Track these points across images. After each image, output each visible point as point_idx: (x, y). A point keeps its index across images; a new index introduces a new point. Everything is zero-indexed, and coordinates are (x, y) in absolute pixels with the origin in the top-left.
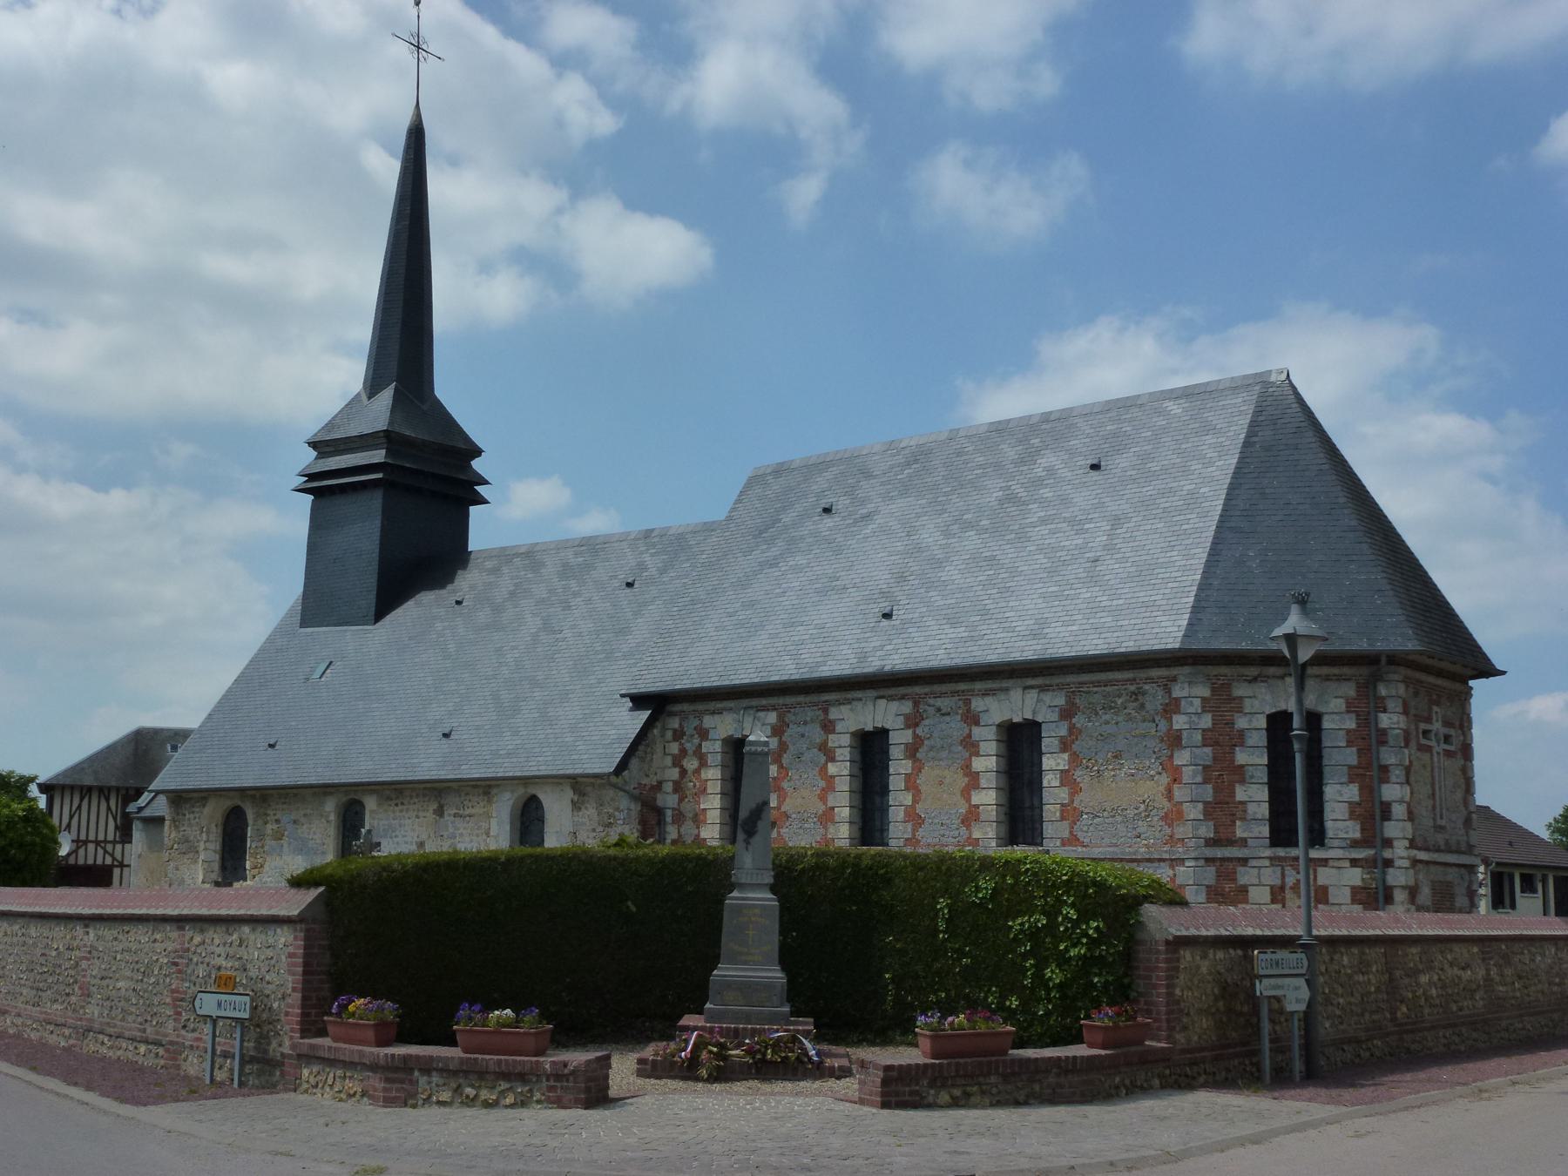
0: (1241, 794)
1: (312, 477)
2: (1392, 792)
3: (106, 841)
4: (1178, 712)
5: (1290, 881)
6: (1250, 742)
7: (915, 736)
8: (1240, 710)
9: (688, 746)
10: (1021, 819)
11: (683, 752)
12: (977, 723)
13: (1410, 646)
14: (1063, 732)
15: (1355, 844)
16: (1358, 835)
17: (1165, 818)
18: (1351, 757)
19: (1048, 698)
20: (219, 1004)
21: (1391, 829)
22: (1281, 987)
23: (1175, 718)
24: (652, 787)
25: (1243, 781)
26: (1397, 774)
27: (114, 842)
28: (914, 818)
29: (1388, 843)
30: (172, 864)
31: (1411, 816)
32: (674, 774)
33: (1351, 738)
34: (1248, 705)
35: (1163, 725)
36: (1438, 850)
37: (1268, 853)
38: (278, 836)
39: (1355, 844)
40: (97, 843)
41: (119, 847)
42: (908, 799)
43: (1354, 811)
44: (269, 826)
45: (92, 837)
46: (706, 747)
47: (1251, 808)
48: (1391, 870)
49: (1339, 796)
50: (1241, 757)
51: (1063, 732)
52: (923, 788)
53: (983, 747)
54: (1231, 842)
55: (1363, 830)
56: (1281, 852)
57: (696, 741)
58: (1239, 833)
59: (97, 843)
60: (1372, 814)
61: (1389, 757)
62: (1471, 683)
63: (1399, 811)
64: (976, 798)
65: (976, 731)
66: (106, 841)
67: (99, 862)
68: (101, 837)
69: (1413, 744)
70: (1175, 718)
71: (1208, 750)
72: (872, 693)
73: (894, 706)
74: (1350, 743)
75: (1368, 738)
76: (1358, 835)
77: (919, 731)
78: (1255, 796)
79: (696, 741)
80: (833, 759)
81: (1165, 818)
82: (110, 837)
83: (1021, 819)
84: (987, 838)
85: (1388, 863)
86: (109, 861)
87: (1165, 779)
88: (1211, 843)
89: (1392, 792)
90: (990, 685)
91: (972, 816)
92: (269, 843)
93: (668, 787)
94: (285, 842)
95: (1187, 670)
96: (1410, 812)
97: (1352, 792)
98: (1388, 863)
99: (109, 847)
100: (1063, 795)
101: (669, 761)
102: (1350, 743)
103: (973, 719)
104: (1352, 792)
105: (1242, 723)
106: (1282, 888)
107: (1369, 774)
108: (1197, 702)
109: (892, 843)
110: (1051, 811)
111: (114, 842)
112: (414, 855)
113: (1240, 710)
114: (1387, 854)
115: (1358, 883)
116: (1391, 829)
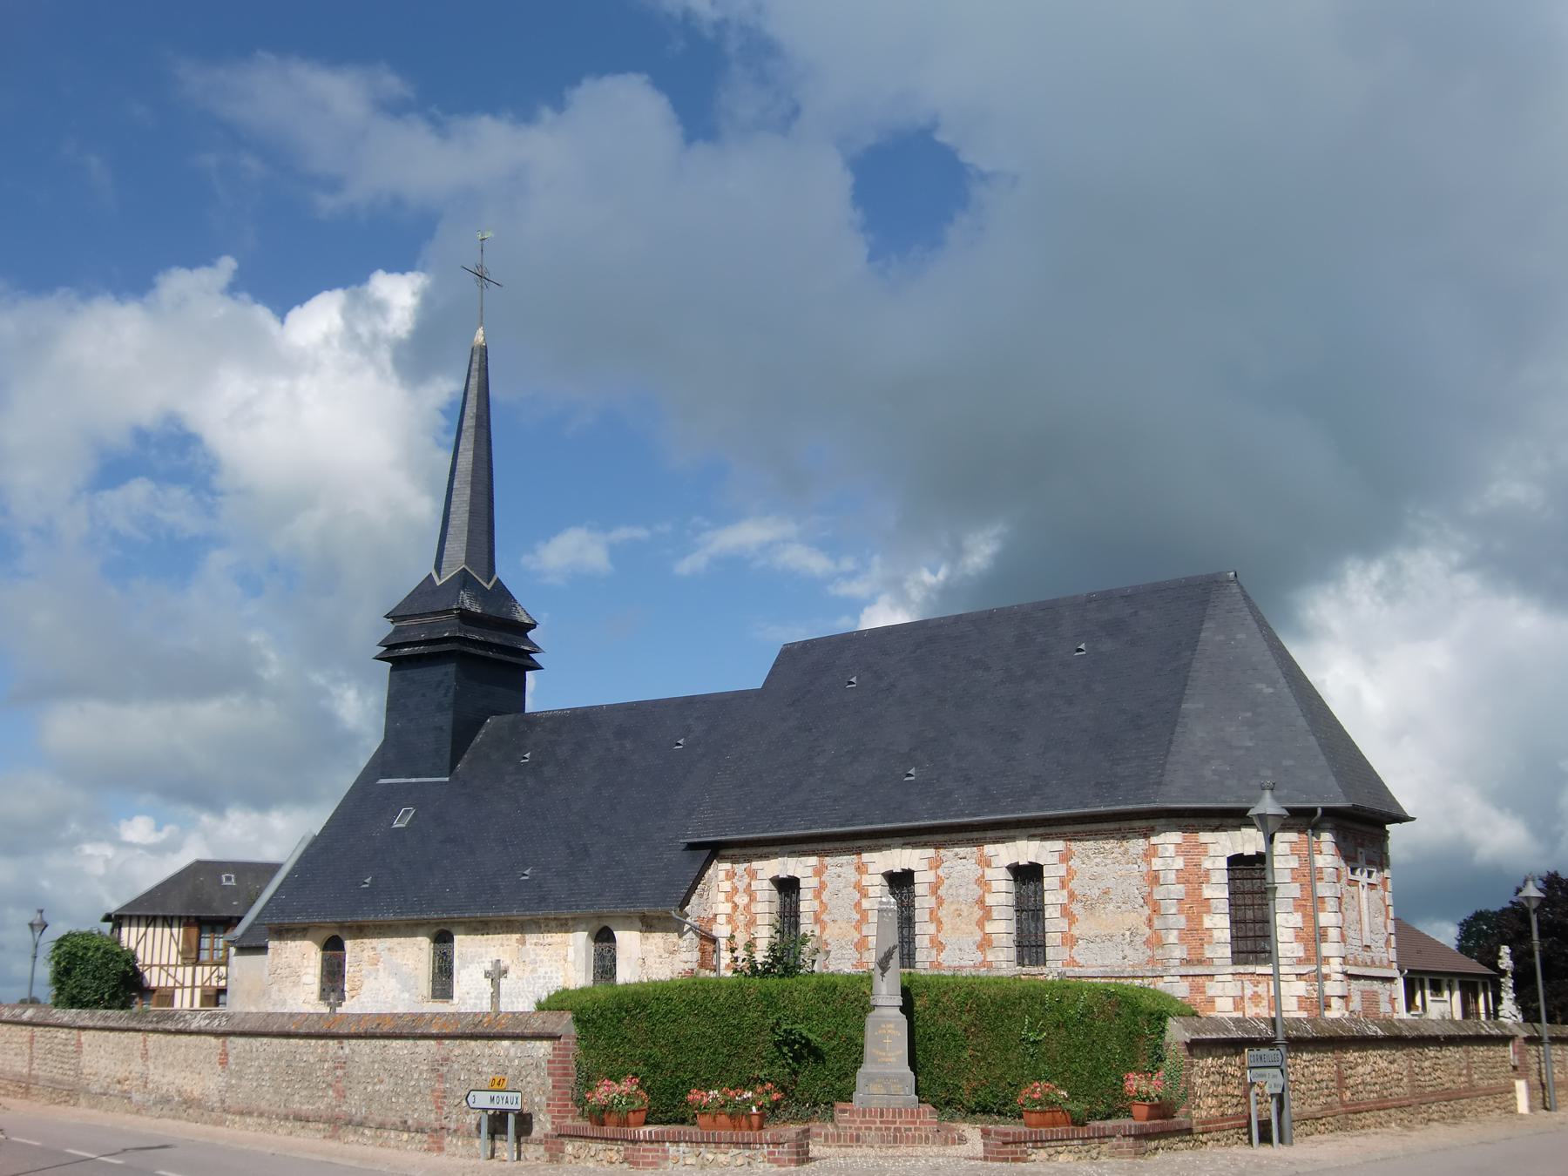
0: (1208, 922)
1: (391, 647)
2: (1327, 918)
3: (168, 965)
4: (1155, 855)
5: (1248, 992)
6: (1214, 880)
7: (938, 877)
8: (1205, 853)
9: (738, 884)
10: (1030, 945)
11: (735, 890)
12: (989, 866)
13: (981, 551)
14: (1062, 872)
15: (1300, 961)
16: (1301, 954)
17: (1147, 942)
18: (1295, 890)
19: (1049, 845)
20: (492, 1099)
21: (1327, 949)
22: (1263, 1075)
23: (1154, 860)
24: (709, 920)
25: (1208, 912)
26: (1331, 904)
27: (177, 966)
28: (938, 945)
29: (1326, 960)
30: (275, 987)
31: (1343, 939)
32: (727, 908)
33: (1296, 874)
34: (1212, 849)
35: (1144, 868)
36: (1366, 965)
37: (1231, 969)
38: (375, 962)
39: (1300, 961)
40: (161, 967)
41: (180, 969)
42: (932, 929)
43: (1299, 934)
44: (366, 954)
45: (156, 961)
46: (755, 885)
47: (1216, 933)
48: (1327, 983)
49: (1286, 923)
50: (1207, 892)
51: (1062, 872)
52: (944, 920)
53: (995, 886)
54: (1200, 962)
55: (1306, 950)
56: (1241, 969)
57: (746, 880)
58: (1208, 955)
59: (161, 967)
60: (1314, 936)
61: (1323, 889)
62: (1388, 827)
63: (1333, 934)
64: (990, 927)
65: (988, 871)
66: (168, 965)
67: (163, 984)
68: (164, 962)
69: (1344, 881)
70: (1154, 860)
71: (1181, 886)
72: (901, 840)
73: (918, 853)
74: (1294, 880)
75: (1307, 876)
76: (1301, 954)
77: (940, 872)
78: (1219, 924)
79: (746, 880)
80: (866, 896)
81: (1147, 942)
82: (173, 961)
83: (1030, 945)
84: (1003, 961)
85: (1326, 977)
86: (171, 983)
87: (1147, 911)
88: (1189, 962)
89: (1327, 918)
90: (999, 834)
91: (985, 943)
92: (366, 968)
93: (721, 919)
94: (381, 965)
95: (1163, 821)
96: (1342, 935)
97: (1297, 919)
98: (1326, 977)
99: (172, 971)
100: (1063, 924)
101: (722, 897)
102: (1294, 880)
103: (986, 863)
104: (1297, 919)
105: (1207, 864)
106: (1242, 998)
107: (1310, 904)
108: (1171, 848)
109: (918, 965)
110: (1052, 939)
111: (177, 966)
112: (1342, 1027)
113: (1205, 853)
114: (1325, 970)
115: (1303, 993)
116: (1327, 949)
